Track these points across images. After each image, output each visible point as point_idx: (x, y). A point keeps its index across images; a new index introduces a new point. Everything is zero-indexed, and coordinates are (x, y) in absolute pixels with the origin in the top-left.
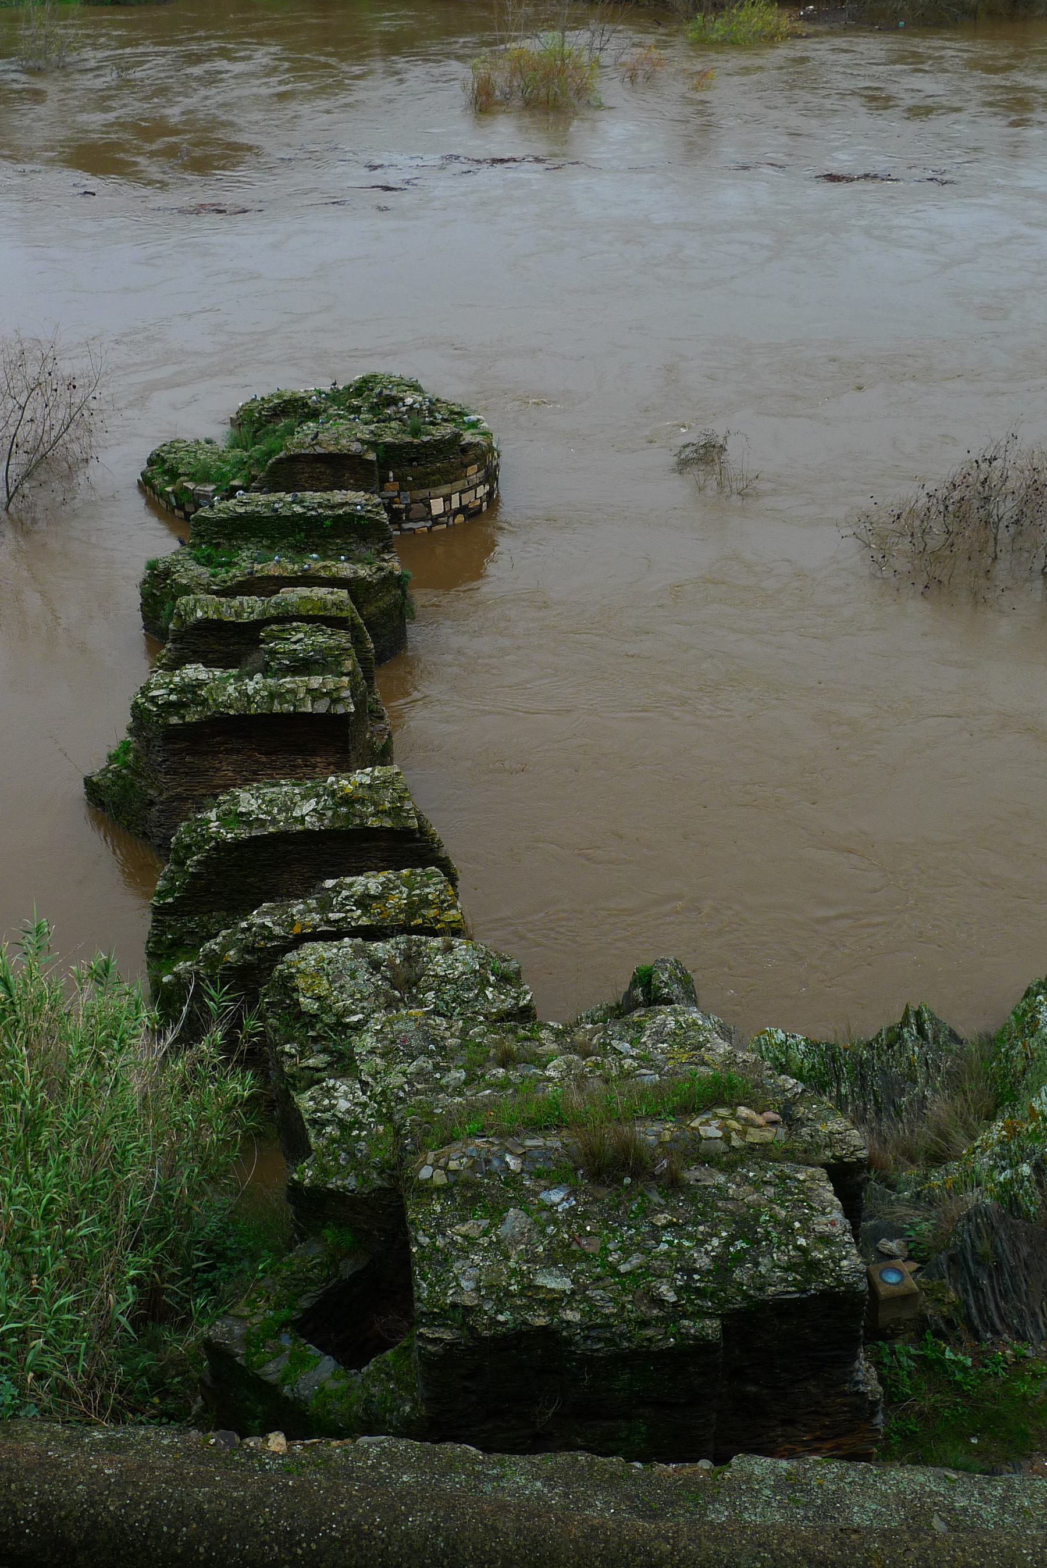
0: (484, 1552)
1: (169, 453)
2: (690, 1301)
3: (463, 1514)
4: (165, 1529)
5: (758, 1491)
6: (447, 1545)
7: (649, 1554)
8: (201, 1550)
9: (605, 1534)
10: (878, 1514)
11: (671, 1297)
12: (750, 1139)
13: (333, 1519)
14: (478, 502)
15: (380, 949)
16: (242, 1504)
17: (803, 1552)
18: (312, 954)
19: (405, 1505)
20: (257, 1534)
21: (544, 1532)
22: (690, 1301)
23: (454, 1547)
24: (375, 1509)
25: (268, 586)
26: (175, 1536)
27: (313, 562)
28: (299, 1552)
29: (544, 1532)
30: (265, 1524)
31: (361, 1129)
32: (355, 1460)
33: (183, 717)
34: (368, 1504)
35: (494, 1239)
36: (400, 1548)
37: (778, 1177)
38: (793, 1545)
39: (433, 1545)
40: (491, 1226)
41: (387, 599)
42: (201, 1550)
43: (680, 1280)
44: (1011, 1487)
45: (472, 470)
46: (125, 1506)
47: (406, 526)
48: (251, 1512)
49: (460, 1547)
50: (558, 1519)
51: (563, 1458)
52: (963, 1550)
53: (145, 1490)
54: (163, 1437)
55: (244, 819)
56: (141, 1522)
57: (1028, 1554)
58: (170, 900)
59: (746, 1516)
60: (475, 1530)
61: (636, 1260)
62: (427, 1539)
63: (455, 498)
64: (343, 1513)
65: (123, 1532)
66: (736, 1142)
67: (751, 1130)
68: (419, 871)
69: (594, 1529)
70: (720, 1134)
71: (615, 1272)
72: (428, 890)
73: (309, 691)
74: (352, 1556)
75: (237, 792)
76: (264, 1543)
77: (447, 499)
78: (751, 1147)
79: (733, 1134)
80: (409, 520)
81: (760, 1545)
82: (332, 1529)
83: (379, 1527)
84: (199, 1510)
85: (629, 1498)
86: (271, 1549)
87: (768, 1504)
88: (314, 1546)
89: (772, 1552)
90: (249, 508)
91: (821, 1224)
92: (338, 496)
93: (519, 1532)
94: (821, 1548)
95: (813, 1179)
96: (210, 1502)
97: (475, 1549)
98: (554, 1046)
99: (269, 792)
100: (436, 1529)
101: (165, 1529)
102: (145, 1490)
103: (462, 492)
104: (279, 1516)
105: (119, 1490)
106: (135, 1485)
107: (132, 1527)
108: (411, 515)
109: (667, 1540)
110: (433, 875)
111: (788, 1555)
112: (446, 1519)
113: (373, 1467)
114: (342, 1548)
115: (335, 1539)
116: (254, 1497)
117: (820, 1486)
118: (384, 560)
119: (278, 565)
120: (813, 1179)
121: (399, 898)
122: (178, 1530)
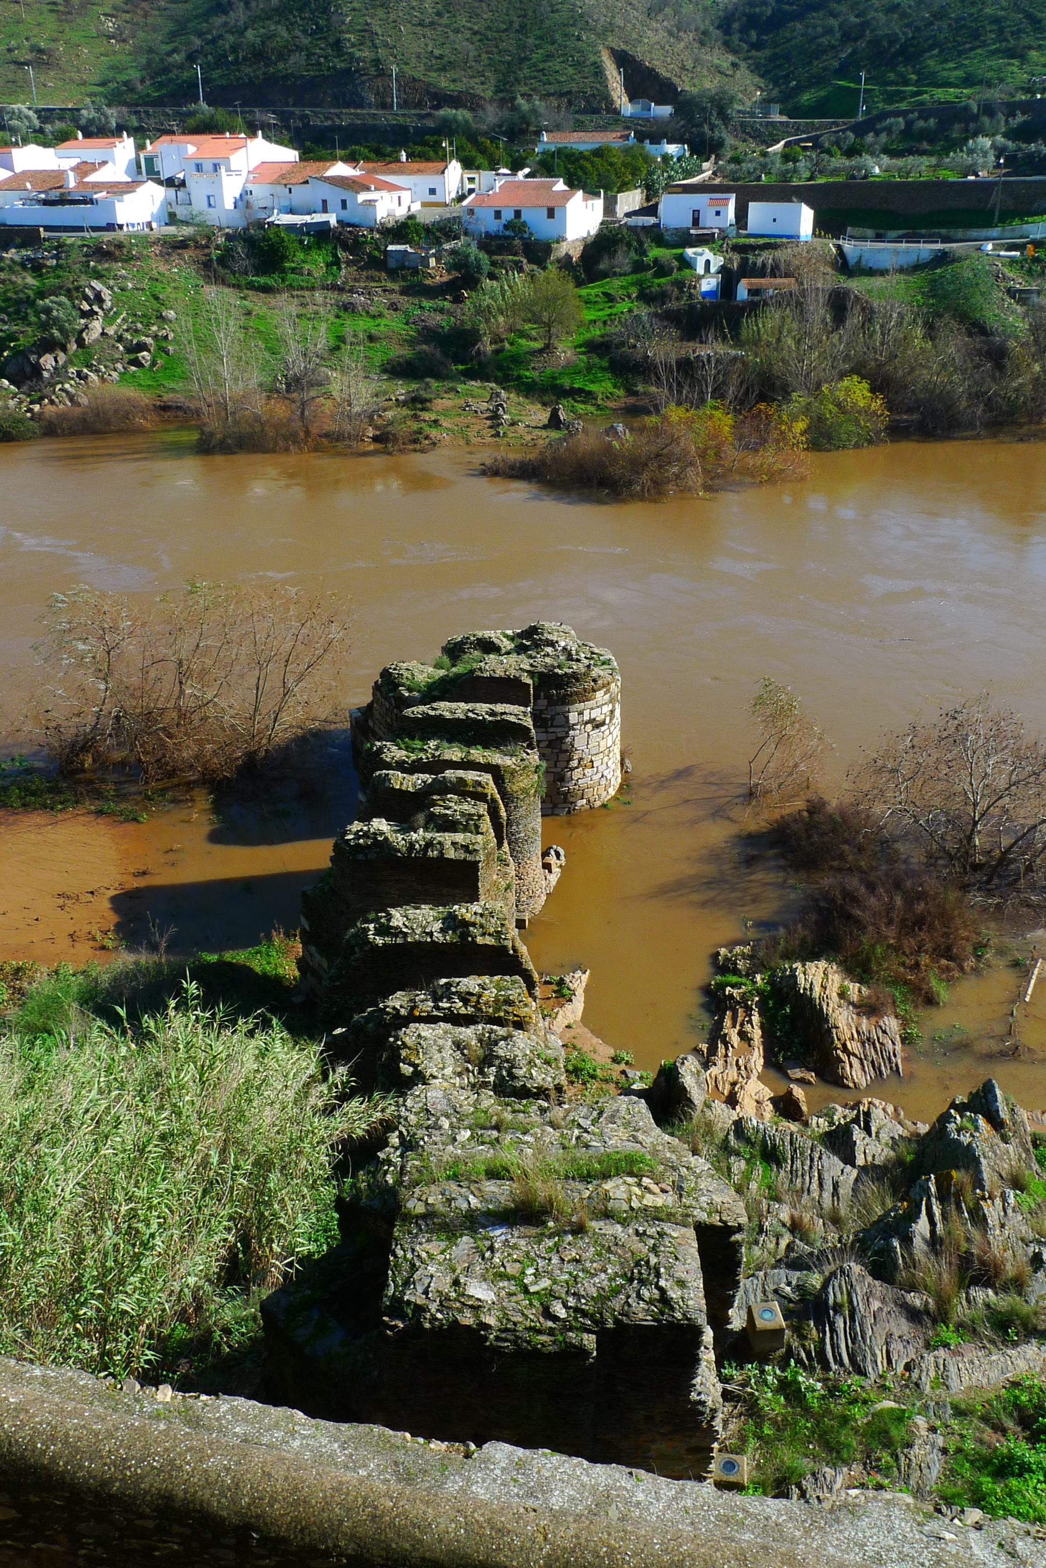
0: (258, 1491)
1: (395, 669)
2: (576, 1319)
3: (250, 1461)
4: (39, 1445)
5: (492, 1470)
6: (233, 1482)
7: (376, 1508)
8: (61, 1463)
9: (347, 1488)
10: (572, 1499)
11: (562, 1313)
12: (645, 1202)
13: (157, 1454)
14: (603, 717)
15: (468, 1033)
16: (96, 1435)
17: (489, 1521)
18: (426, 1030)
19: (212, 1449)
20: (101, 1457)
21: (303, 1482)
22: (576, 1319)
23: (237, 1484)
24: (189, 1449)
25: (437, 766)
26: (45, 1451)
27: (477, 754)
28: (128, 1473)
29: (303, 1482)
30: (110, 1451)
31: (389, 1165)
32: (209, 1412)
33: (366, 855)
34: (186, 1445)
35: (448, 1257)
36: (199, 1480)
37: (658, 1233)
38: (483, 1515)
39: (222, 1481)
40: (447, 1248)
41: (525, 781)
42: (61, 1463)
43: (572, 1302)
44: (682, 1490)
45: (599, 694)
46: (15, 1426)
47: (551, 730)
48: (102, 1440)
49: (241, 1484)
50: (318, 1473)
51: (363, 1428)
52: (609, 1534)
53: (34, 1416)
54: (82, 1379)
55: (397, 932)
56: (24, 1438)
57: (657, 1544)
58: (337, 983)
59: (474, 1487)
60: (255, 1474)
61: (545, 1283)
62: (219, 1476)
63: (586, 713)
64: (166, 1450)
65: (10, 1444)
66: (635, 1204)
67: (648, 1195)
68: (507, 978)
69: (341, 1483)
70: (625, 1196)
71: (525, 1290)
72: (510, 992)
73: (453, 844)
74: (164, 1481)
75: (393, 911)
76: (105, 1464)
77: (581, 713)
78: (646, 1209)
79: (634, 1197)
80: (552, 726)
81: (458, 1511)
82: (154, 1460)
83: (188, 1463)
84: (67, 1435)
85: (396, 1463)
86: (109, 1469)
87: (495, 1480)
88: (139, 1471)
89: (466, 1517)
90: (438, 713)
91: (680, 1272)
92: (499, 708)
93: (286, 1478)
94: (503, 1519)
95: (683, 1236)
96: (75, 1430)
97: (251, 1487)
98: (538, 1119)
99: (411, 912)
100: (228, 1469)
101: (39, 1445)
102: (34, 1416)
103: (592, 709)
104: (120, 1446)
105: (14, 1414)
106: (27, 1411)
107: (17, 1441)
108: (555, 723)
109: (391, 1498)
110: (514, 982)
111: (477, 1521)
112: (238, 1463)
113: (218, 1419)
114: (158, 1475)
115: (156, 1468)
116: (107, 1430)
117: (538, 1472)
118: (528, 754)
119: (455, 753)
120: (683, 1236)
121: (490, 995)
122: (48, 1448)
